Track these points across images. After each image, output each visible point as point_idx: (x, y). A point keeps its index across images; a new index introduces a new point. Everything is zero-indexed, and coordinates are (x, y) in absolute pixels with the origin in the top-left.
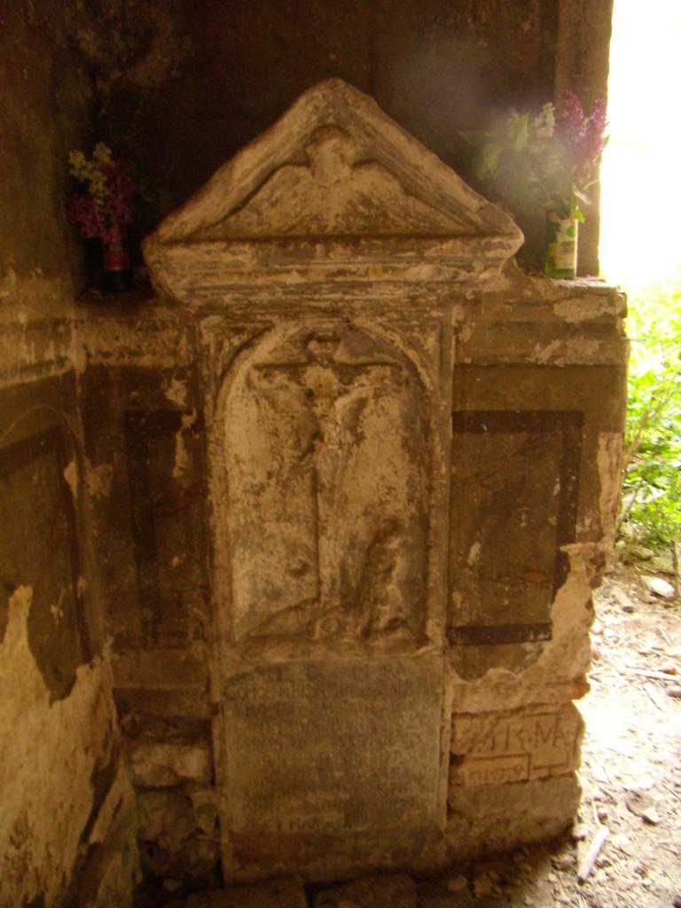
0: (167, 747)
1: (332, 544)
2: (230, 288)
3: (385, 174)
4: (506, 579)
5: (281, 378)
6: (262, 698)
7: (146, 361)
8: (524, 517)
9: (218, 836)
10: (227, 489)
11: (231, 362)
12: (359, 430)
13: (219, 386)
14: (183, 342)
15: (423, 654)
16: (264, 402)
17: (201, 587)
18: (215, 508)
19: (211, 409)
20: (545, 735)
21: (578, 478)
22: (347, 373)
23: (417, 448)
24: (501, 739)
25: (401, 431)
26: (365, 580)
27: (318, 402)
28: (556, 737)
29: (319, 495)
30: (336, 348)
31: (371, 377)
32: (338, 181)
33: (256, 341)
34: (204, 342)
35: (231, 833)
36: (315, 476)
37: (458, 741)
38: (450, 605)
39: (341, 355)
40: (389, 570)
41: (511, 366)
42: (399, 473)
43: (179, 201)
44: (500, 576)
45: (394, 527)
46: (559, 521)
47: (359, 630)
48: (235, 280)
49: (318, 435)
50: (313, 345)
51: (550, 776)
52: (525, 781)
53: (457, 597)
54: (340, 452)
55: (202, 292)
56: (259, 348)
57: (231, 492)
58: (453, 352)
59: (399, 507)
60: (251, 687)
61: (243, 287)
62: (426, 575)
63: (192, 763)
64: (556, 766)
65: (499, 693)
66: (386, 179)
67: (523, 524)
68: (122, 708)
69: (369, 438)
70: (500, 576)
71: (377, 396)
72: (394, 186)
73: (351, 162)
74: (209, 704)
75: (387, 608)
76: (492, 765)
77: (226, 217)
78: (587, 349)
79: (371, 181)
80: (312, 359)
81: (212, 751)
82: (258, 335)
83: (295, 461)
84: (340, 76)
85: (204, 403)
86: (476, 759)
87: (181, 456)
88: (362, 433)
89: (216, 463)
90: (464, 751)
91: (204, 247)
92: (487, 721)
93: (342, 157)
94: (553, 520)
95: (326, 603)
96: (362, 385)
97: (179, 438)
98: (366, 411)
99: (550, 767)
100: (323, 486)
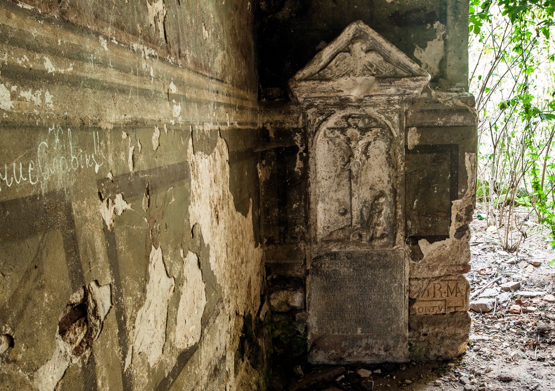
0: (285, 292)
1: (357, 201)
2: (319, 98)
3: (378, 55)
4: (430, 215)
5: (337, 133)
6: (328, 267)
7: (287, 126)
8: (436, 188)
9: (306, 335)
10: (316, 176)
11: (319, 126)
12: (368, 154)
13: (314, 136)
14: (301, 118)
15: (396, 249)
16: (330, 142)
17: (304, 217)
18: (311, 184)
19: (311, 144)
20: (452, 291)
21: (458, 172)
22: (364, 131)
23: (391, 162)
24: (432, 291)
25: (385, 154)
26: (371, 217)
27: (352, 142)
28: (457, 292)
29: (352, 181)
30: (359, 121)
31: (372, 132)
32: (360, 58)
33: (328, 118)
34: (309, 118)
35: (312, 334)
36: (350, 171)
37: (412, 291)
38: (406, 226)
39: (361, 125)
40: (380, 212)
41: (428, 127)
42: (384, 172)
43: (302, 66)
44: (427, 214)
45: (382, 194)
46: (451, 190)
47: (368, 238)
48: (323, 94)
49: (352, 155)
50: (350, 120)
51: (455, 312)
52: (444, 314)
53: (409, 223)
54: (360, 163)
55: (309, 99)
56: (330, 121)
57: (317, 178)
58: (405, 122)
59: (386, 187)
60: (323, 262)
61: (325, 97)
62: (396, 213)
63: (297, 300)
64: (458, 307)
65: (429, 269)
66: (378, 56)
67: (436, 191)
68: (268, 272)
69: (371, 157)
70: (427, 214)
71: (375, 140)
72: (381, 59)
73: (365, 51)
74: (306, 270)
75: (380, 228)
76: (428, 304)
77: (319, 71)
78: (459, 119)
79: (373, 57)
80: (349, 126)
81: (305, 293)
82: (329, 115)
83: (342, 167)
84: (361, 19)
85: (308, 142)
86: (420, 301)
87: (299, 164)
88: (369, 156)
89: (312, 167)
90: (415, 297)
91: (311, 82)
92: (425, 282)
93: (362, 49)
94: (448, 190)
95: (354, 226)
96: (369, 136)
97: (298, 156)
98: (370, 147)
99: (455, 307)
100: (354, 177)
